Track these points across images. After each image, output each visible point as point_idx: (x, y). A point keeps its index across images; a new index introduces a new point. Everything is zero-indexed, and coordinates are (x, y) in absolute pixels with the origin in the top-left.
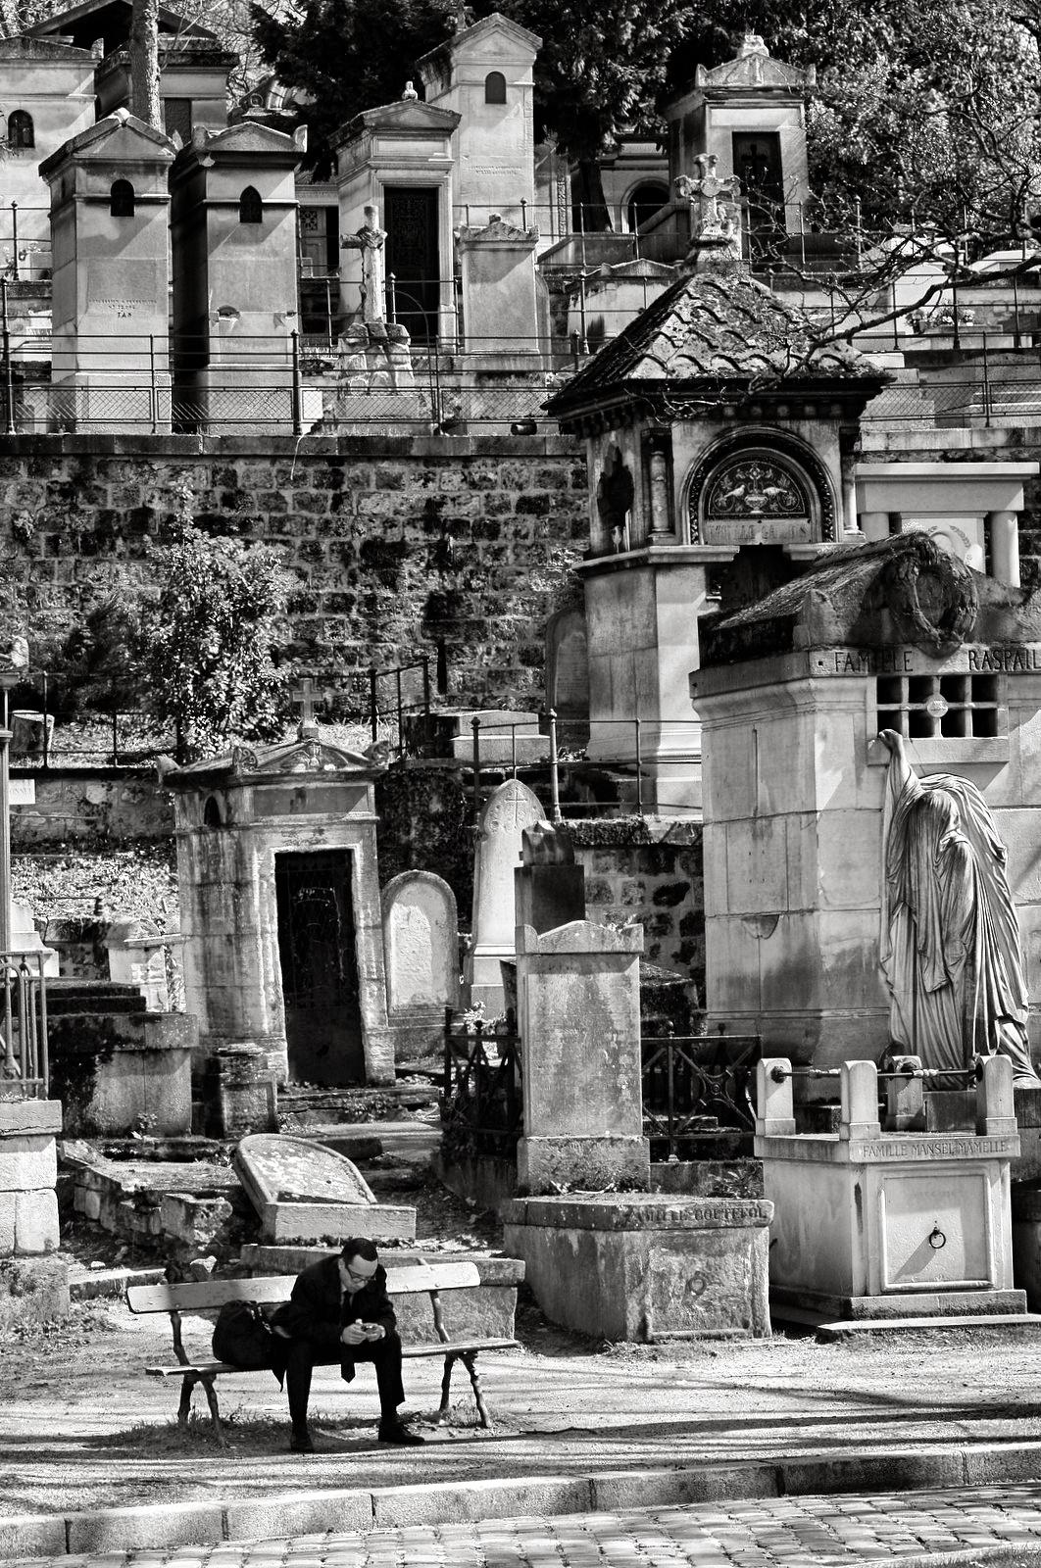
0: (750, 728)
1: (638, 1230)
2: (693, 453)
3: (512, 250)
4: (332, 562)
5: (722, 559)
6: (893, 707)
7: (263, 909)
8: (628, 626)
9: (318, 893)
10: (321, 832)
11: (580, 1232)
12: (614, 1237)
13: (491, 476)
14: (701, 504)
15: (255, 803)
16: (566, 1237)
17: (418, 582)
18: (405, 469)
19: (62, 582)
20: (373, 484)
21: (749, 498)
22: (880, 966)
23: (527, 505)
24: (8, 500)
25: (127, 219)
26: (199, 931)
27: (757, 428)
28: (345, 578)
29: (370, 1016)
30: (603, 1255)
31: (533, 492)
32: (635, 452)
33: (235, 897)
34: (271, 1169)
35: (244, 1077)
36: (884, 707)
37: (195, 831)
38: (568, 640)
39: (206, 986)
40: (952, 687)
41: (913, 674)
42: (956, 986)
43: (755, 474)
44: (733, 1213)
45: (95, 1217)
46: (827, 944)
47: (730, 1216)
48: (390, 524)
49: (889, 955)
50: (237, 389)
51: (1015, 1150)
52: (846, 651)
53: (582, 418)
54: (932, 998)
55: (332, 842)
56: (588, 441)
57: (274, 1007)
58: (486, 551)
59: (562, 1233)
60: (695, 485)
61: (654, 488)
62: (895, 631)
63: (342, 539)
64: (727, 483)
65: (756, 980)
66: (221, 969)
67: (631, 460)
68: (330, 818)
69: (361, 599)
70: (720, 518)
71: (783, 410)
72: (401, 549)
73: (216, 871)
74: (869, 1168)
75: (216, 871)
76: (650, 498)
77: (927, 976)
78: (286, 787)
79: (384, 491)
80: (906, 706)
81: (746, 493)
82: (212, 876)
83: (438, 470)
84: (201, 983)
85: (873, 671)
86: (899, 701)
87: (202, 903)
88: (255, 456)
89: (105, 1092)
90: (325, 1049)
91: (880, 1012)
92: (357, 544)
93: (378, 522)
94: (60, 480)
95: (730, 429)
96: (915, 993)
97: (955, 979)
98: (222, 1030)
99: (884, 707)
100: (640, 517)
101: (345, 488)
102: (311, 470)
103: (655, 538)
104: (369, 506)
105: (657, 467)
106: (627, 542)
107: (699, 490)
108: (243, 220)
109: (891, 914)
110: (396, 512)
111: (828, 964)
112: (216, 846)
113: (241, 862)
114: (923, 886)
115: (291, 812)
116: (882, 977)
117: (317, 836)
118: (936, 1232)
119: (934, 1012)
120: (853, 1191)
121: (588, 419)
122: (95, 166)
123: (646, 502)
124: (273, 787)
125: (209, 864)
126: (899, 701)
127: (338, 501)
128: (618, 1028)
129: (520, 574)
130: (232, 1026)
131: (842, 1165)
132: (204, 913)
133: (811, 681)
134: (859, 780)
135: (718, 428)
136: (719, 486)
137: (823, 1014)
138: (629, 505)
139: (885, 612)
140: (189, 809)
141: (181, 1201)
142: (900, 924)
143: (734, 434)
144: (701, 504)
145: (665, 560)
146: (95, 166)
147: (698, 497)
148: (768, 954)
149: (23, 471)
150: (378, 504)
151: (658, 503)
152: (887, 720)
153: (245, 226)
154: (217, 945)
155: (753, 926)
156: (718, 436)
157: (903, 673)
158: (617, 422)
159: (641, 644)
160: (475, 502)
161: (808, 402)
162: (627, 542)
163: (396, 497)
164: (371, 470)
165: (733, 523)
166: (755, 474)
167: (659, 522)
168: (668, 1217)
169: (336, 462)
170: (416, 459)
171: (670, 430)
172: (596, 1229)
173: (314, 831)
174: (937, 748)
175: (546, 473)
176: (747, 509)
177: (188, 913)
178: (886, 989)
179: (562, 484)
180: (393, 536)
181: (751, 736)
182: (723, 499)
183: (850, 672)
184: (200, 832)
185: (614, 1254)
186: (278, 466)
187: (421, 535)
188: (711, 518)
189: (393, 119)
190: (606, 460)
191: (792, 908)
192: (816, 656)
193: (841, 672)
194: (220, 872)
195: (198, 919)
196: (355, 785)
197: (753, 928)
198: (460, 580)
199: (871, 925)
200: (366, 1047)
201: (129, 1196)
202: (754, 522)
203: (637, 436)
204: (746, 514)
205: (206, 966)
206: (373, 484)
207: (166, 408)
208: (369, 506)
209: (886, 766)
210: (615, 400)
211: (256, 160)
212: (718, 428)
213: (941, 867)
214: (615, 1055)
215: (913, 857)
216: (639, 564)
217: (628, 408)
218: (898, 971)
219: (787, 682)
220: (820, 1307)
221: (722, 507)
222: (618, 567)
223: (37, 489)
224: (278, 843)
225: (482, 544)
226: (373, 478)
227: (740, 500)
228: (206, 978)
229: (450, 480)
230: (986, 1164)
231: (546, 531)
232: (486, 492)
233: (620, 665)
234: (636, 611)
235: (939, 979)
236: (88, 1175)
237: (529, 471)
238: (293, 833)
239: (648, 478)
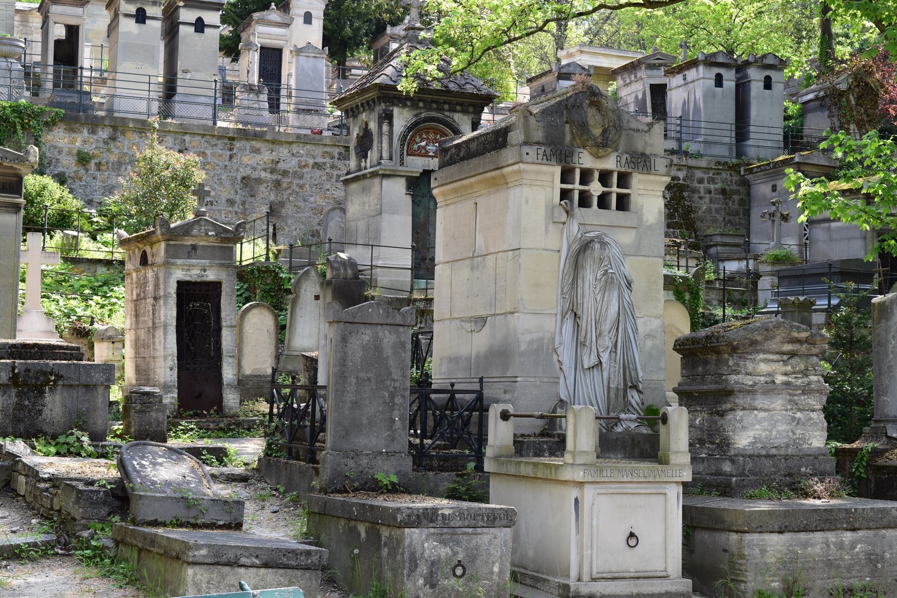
0: (473, 201)
1: (417, 527)
2: (404, 123)
3: (316, 57)
4: (227, 184)
5: (415, 175)
8: (367, 206)
9: (202, 306)
10: (205, 270)
11: (367, 524)
12: (396, 532)
13: (301, 151)
14: (405, 148)
15: (167, 251)
16: (356, 527)
17: (266, 194)
18: (263, 145)
19: (101, 184)
20: (248, 150)
21: (428, 147)
22: (555, 350)
23: (317, 166)
24: (77, 144)
25: (142, 25)
26: (134, 327)
27: (434, 114)
28: (232, 192)
29: (228, 373)
30: (386, 544)
31: (320, 160)
32: (375, 121)
33: (154, 305)
34: (142, 466)
35: (738, 575)
36: (565, 186)
37: (134, 270)
38: (334, 221)
39: (136, 357)
40: (605, 177)
41: (583, 166)
42: (604, 365)
43: (431, 136)
44: (488, 517)
45: (22, 494)
46: (523, 334)
47: (485, 518)
48: (254, 169)
49: (561, 344)
50: (190, 103)
51: (687, 476)
52: (543, 148)
53: (349, 108)
54: (587, 372)
55: (211, 276)
56: (351, 119)
57: (171, 369)
58: (298, 185)
59: (352, 523)
60: (403, 138)
61: (383, 138)
62: (573, 138)
63: (232, 174)
64: (418, 139)
65: (469, 359)
66: (144, 347)
67: (373, 126)
68: (210, 263)
69: (240, 202)
70: (414, 155)
71: (446, 107)
72: (259, 181)
73: (144, 292)
74: (586, 486)
75: (144, 292)
76: (381, 143)
77: (586, 359)
78: (186, 243)
79: (252, 154)
80: (577, 186)
81: (427, 145)
82: (142, 295)
83: (278, 147)
84: (133, 356)
86: (573, 183)
87: (136, 310)
88: (195, 134)
89: (51, 410)
90: (200, 395)
91: (553, 380)
92: (239, 178)
93: (249, 168)
94: (103, 137)
95: (421, 113)
96: (576, 369)
97: (604, 359)
98: (143, 382)
99: (565, 186)
100: (376, 152)
101: (235, 151)
102: (220, 142)
103: (382, 161)
104: (245, 160)
105: (385, 128)
106: (368, 165)
107: (405, 141)
108: (196, 31)
109: (563, 317)
110: (257, 164)
111: (523, 348)
112: (145, 278)
114: (586, 300)
115: (188, 258)
116: (555, 357)
117: (203, 272)
118: (632, 535)
119: (588, 381)
120: (573, 501)
121: (352, 109)
123: (379, 145)
124: (178, 243)
125: (141, 288)
126: (573, 183)
127: (231, 157)
128: (395, 377)
129: (311, 196)
130: (148, 380)
131: (565, 482)
132: (137, 316)
133: (521, 164)
134: (547, 231)
135: (416, 112)
136: (414, 140)
137: (518, 379)
138: (370, 147)
139: (567, 126)
140: (133, 258)
141: (73, 487)
142: (569, 324)
143: (423, 116)
144: (405, 148)
145: (387, 173)
147: (404, 144)
148: (480, 342)
149: (85, 131)
150: (248, 159)
151: (385, 145)
153: (196, 33)
154: (142, 334)
155: (469, 325)
156: (416, 115)
157: (577, 165)
158: (367, 107)
159: (373, 214)
160: (293, 162)
161: (458, 104)
162: (368, 165)
163: (258, 157)
164: (248, 145)
165: (420, 158)
166: (431, 136)
167: (385, 155)
168: (440, 518)
169: (232, 139)
170: (268, 141)
171: (392, 111)
172: (381, 524)
173: (201, 270)
174: (593, 213)
175: (327, 152)
176: (427, 152)
177: (129, 317)
178: (557, 365)
179: (333, 157)
180: (255, 175)
181: (472, 206)
182: (415, 147)
183: (545, 161)
184: (137, 271)
185: (396, 545)
186: (205, 139)
187: (269, 175)
188: (410, 155)
189: (265, 17)
190: (360, 127)
191: (497, 312)
193: (540, 161)
194: (146, 292)
195: (134, 319)
196: (226, 245)
197: (468, 326)
198: (285, 197)
199: (550, 324)
200: (224, 395)
201: (45, 480)
202: (430, 159)
203: (377, 114)
204: (426, 155)
205: (136, 346)
206: (248, 150)
207: (155, 107)
208: (245, 160)
209: (564, 223)
210: (366, 96)
211: (203, 5)
212: (416, 112)
213: (598, 288)
214: (392, 396)
215: (580, 281)
216: (374, 175)
217: (373, 100)
218: (566, 355)
219: (502, 167)
220: (539, 585)
221: (415, 151)
222: (364, 177)
223: (92, 140)
224: (179, 275)
225: (296, 181)
226: (248, 148)
227: (424, 148)
228: (136, 353)
229: (284, 152)
230: (667, 486)
231: (324, 178)
232: (298, 158)
233: (362, 225)
234: (371, 198)
235: (594, 360)
236: (20, 465)
237: (319, 151)
238: (188, 270)
239: (381, 134)
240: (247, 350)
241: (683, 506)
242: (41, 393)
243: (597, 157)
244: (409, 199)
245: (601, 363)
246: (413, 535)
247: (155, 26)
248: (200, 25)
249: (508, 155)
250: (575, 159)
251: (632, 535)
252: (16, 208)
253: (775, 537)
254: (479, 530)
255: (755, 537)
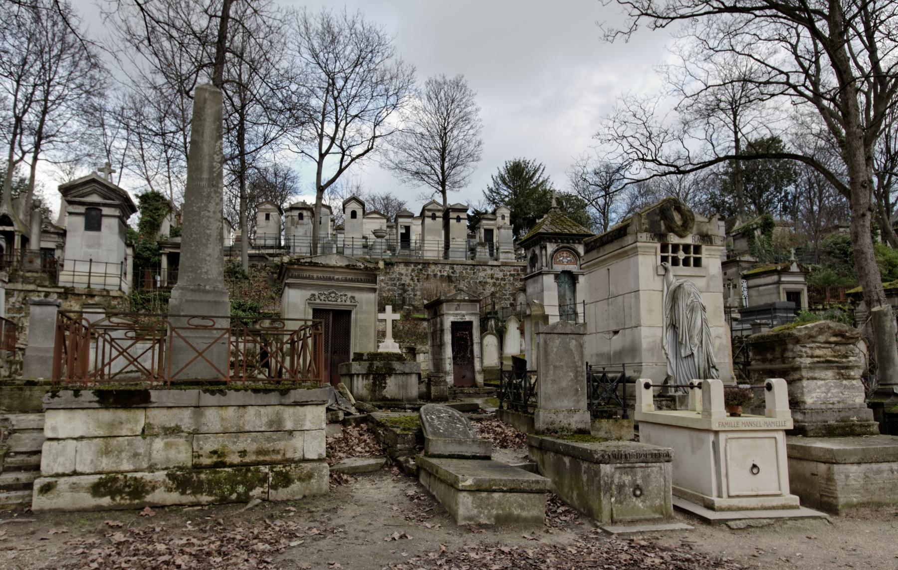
6: (666, 254)
7: (448, 338)
29: (477, 366)
34: (432, 419)
40: (686, 248)
55: (467, 319)
72: (486, 283)
85: (659, 241)
90: (464, 377)
97: (695, 352)
113: (442, 324)
118: (754, 466)
122: (429, 210)
146: (429, 210)
150: (482, 274)
151: (544, 260)
152: (664, 259)
167: (544, 264)
174: (681, 269)
192: (639, 235)
207: (441, 254)
235: (689, 352)
239: (541, 255)
240: (486, 354)
241: (787, 445)
242: (384, 379)
243: (681, 236)
244: (556, 284)
245: (693, 354)
246: (606, 469)
247: (440, 221)
248: (458, 219)
249: (629, 239)
250: (668, 238)
251: (754, 466)
252: (374, 290)
253: (855, 468)
254: (650, 465)
255: (841, 467)
